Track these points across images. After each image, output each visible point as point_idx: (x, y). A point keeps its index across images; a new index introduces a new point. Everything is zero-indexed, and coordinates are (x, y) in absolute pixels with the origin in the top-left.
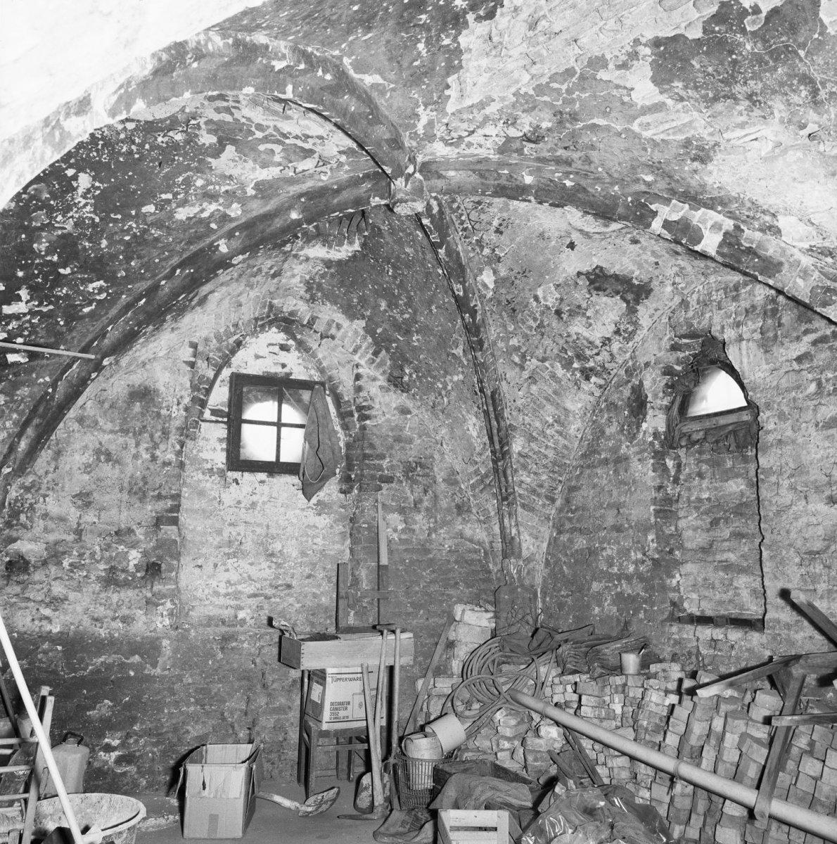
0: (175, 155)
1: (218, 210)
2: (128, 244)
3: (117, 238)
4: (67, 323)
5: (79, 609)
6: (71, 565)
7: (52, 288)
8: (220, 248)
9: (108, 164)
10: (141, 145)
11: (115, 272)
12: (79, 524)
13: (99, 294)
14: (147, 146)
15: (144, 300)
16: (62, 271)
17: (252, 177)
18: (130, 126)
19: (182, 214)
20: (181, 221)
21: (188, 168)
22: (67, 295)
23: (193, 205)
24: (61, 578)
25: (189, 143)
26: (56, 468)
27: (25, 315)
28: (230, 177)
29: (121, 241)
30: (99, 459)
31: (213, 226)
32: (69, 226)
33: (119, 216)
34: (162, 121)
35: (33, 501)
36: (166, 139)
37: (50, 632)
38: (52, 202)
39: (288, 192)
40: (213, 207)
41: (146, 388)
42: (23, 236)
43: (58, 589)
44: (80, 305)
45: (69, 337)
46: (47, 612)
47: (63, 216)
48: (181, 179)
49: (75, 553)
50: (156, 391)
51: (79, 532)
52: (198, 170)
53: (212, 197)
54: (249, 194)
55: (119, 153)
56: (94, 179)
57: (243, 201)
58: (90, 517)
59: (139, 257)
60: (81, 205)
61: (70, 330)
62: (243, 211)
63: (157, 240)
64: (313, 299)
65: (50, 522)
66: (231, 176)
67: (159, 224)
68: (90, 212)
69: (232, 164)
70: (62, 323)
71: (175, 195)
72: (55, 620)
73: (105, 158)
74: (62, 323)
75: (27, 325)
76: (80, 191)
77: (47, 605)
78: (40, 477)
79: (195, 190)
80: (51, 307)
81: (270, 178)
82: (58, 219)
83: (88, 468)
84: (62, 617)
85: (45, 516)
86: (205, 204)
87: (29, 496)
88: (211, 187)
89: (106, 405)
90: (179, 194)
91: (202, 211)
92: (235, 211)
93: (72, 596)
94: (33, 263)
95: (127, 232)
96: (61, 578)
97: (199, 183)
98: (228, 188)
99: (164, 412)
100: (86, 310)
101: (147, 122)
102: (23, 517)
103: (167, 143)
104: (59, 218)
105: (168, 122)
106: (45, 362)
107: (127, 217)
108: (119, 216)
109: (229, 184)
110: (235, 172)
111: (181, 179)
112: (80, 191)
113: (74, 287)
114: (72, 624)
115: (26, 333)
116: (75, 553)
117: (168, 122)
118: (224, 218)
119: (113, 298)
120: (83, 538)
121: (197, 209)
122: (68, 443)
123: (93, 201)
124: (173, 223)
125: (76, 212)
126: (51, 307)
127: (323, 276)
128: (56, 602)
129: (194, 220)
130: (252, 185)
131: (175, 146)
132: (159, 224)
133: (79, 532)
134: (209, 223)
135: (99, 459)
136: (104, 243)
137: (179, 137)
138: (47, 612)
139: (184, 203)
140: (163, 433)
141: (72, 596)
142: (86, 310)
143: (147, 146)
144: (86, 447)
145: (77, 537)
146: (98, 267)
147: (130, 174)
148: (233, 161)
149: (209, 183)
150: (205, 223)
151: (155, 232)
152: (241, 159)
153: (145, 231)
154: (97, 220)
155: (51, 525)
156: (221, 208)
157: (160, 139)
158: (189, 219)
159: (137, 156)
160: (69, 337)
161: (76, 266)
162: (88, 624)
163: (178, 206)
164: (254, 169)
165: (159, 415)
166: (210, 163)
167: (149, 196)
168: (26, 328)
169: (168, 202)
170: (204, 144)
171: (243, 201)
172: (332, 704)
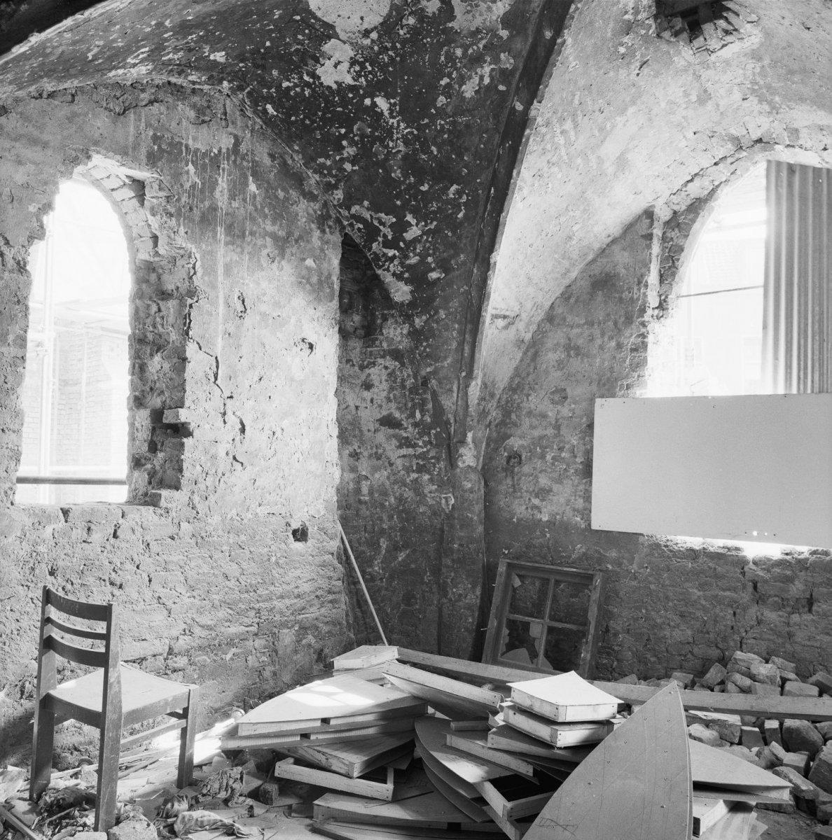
0: (422, 40)
1: (493, 70)
2: (450, 142)
3: (439, 140)
4: (454, 233)
5: (562, 500)
6: (553, 458)
7: (426, 206)
8: (517, 107)
9: (385, 78)
10: (394, 48)
11: (459, 173)
12: (557, 420)
13: (460, 197)
14: (398, 45)
15: (493, 189)
16: (422, 188)
17: (494, 18)
18: (374, 35)
19: (469, 90)
20: (472, 98)
21: (441, 45)
22: (439, 208)
23: (470, 78)
24: (545, 471)
25: (424, 22)
26: (535, 368)
27: (421, 236)
28: (478, 31)
29: (444, 141)
30: (569, 356)
31: (502, 88)
32: (402, 148)
33: (426, 121)
34: (389, 16)
35: (519, 401)
36: (405, 30)
37: (540, 520)
38: (377, 134)
39: (534, 12)
40: (487, 69)
41: (607, 275)
42: (381, 171)
43: (544, 481)
44: (453, 213)
45: (462, 245)
46: (536, 501)
47: (393, 141)
48: (443, 58)
49: (555, 447)
50: (616, 276)
51: (557, 427)
52: (448, 42)
53: (477, 60)
54: (505, 38)
55: (387, 65)
56: (388, 99)
57: (506, 46)
58: (565, 411)
59: (467, 150)
60: (395, 125)
61: (459, 238)
62: (514, 57)
63: (468, 126)
64: (774, 109)
65: (534, 420)
66: (477, 29)
67: (459, 111)
68: (406, 128)
69: (470, 16)
70: (450, 234)
71: (449, 75)
72: (544, 510)
73: (380, 76)
74: (450, 234)
75: (428, 245)
76: (386, 113)
77: (537, 496)
78: (523, 379)
79: (461, 62)
80: (435, 223)
81: (508, 7)
82: (391, 145)
83: (560, 365)
84: (549, 507)
85: (530, 413)
86: (479, 70)
87: (516, 397)
88: (470, 51)
89: (572, 300)
90: (452, 73)
91: (482, 78)
92: (507, 62)
93: (556, 487)
94: (401, 190)
95: (442, 130)
96: (545, 471)
97: (459, 52)
98: (484, 42)
99: (626, 295)
100: (460, 215)
101: (381, 24)
102: (513, 416)
103: (408, 32)
104: (391, 144)
105: (394, 13)
106: (457, 273)
107: (433, 118)
108: (426, 121)
109: (482, 39)
110: (478, 22)
111: (443, 58)
112: (386, 113)
113: (438, 199)
114: (557, 514)
115: (431, 252)
116: (555, 447)
117: (394, 13)
118: (505, 75)
119: (473, 197)
120: (562, 433)
121: (476, 80)
122: (542, 344)
123: (400, 117)
124: (468, 103)
125: (398, 133)
126: (435, 223)
127: (763, 73)
128: (543, 493)
129: (483, 90)
130: (500, 26)
131: (414, 31)
132: (459, 111)
133: (557, 427)
134: (496, 87)
135: (569, 356)
136: (434, 149)
137: (412, 21)
138: (536, 501)
139: (462, 80)
140: (627, 318)
141: (556, 487)
142: (460, 215)
143: (398, 45)
144: (558, 344)
145: (556, 432)
146: (444, 174)
147: (406, 78)
148: (468, 12)
149: (465, 48)
150: (491, 88)
151: (462, 119)
152: (471, 6)
153: (454, 123)
154: (416, 132)
155: (535, 422)
156: (493, 66)
157: (401, 32)
158: (476, 92)
159: (398, 59)
160: (462, 245)
161: (429, 180)
162: (571, 514)
163: (460, 86)
164: (489, 9)
165: (621, 299)
166: (452, 28)
167: (433, 88)
168: (429, 247)
169: (448, 85)
170: (434, 13)
171: (506, 46)
172: (528, 624)
